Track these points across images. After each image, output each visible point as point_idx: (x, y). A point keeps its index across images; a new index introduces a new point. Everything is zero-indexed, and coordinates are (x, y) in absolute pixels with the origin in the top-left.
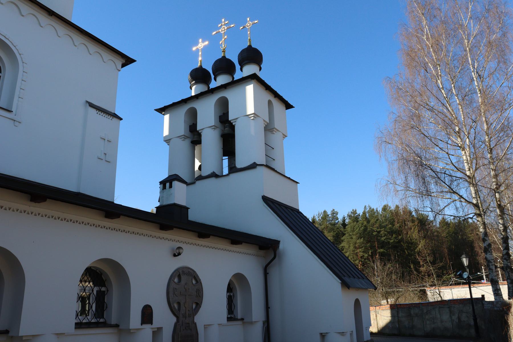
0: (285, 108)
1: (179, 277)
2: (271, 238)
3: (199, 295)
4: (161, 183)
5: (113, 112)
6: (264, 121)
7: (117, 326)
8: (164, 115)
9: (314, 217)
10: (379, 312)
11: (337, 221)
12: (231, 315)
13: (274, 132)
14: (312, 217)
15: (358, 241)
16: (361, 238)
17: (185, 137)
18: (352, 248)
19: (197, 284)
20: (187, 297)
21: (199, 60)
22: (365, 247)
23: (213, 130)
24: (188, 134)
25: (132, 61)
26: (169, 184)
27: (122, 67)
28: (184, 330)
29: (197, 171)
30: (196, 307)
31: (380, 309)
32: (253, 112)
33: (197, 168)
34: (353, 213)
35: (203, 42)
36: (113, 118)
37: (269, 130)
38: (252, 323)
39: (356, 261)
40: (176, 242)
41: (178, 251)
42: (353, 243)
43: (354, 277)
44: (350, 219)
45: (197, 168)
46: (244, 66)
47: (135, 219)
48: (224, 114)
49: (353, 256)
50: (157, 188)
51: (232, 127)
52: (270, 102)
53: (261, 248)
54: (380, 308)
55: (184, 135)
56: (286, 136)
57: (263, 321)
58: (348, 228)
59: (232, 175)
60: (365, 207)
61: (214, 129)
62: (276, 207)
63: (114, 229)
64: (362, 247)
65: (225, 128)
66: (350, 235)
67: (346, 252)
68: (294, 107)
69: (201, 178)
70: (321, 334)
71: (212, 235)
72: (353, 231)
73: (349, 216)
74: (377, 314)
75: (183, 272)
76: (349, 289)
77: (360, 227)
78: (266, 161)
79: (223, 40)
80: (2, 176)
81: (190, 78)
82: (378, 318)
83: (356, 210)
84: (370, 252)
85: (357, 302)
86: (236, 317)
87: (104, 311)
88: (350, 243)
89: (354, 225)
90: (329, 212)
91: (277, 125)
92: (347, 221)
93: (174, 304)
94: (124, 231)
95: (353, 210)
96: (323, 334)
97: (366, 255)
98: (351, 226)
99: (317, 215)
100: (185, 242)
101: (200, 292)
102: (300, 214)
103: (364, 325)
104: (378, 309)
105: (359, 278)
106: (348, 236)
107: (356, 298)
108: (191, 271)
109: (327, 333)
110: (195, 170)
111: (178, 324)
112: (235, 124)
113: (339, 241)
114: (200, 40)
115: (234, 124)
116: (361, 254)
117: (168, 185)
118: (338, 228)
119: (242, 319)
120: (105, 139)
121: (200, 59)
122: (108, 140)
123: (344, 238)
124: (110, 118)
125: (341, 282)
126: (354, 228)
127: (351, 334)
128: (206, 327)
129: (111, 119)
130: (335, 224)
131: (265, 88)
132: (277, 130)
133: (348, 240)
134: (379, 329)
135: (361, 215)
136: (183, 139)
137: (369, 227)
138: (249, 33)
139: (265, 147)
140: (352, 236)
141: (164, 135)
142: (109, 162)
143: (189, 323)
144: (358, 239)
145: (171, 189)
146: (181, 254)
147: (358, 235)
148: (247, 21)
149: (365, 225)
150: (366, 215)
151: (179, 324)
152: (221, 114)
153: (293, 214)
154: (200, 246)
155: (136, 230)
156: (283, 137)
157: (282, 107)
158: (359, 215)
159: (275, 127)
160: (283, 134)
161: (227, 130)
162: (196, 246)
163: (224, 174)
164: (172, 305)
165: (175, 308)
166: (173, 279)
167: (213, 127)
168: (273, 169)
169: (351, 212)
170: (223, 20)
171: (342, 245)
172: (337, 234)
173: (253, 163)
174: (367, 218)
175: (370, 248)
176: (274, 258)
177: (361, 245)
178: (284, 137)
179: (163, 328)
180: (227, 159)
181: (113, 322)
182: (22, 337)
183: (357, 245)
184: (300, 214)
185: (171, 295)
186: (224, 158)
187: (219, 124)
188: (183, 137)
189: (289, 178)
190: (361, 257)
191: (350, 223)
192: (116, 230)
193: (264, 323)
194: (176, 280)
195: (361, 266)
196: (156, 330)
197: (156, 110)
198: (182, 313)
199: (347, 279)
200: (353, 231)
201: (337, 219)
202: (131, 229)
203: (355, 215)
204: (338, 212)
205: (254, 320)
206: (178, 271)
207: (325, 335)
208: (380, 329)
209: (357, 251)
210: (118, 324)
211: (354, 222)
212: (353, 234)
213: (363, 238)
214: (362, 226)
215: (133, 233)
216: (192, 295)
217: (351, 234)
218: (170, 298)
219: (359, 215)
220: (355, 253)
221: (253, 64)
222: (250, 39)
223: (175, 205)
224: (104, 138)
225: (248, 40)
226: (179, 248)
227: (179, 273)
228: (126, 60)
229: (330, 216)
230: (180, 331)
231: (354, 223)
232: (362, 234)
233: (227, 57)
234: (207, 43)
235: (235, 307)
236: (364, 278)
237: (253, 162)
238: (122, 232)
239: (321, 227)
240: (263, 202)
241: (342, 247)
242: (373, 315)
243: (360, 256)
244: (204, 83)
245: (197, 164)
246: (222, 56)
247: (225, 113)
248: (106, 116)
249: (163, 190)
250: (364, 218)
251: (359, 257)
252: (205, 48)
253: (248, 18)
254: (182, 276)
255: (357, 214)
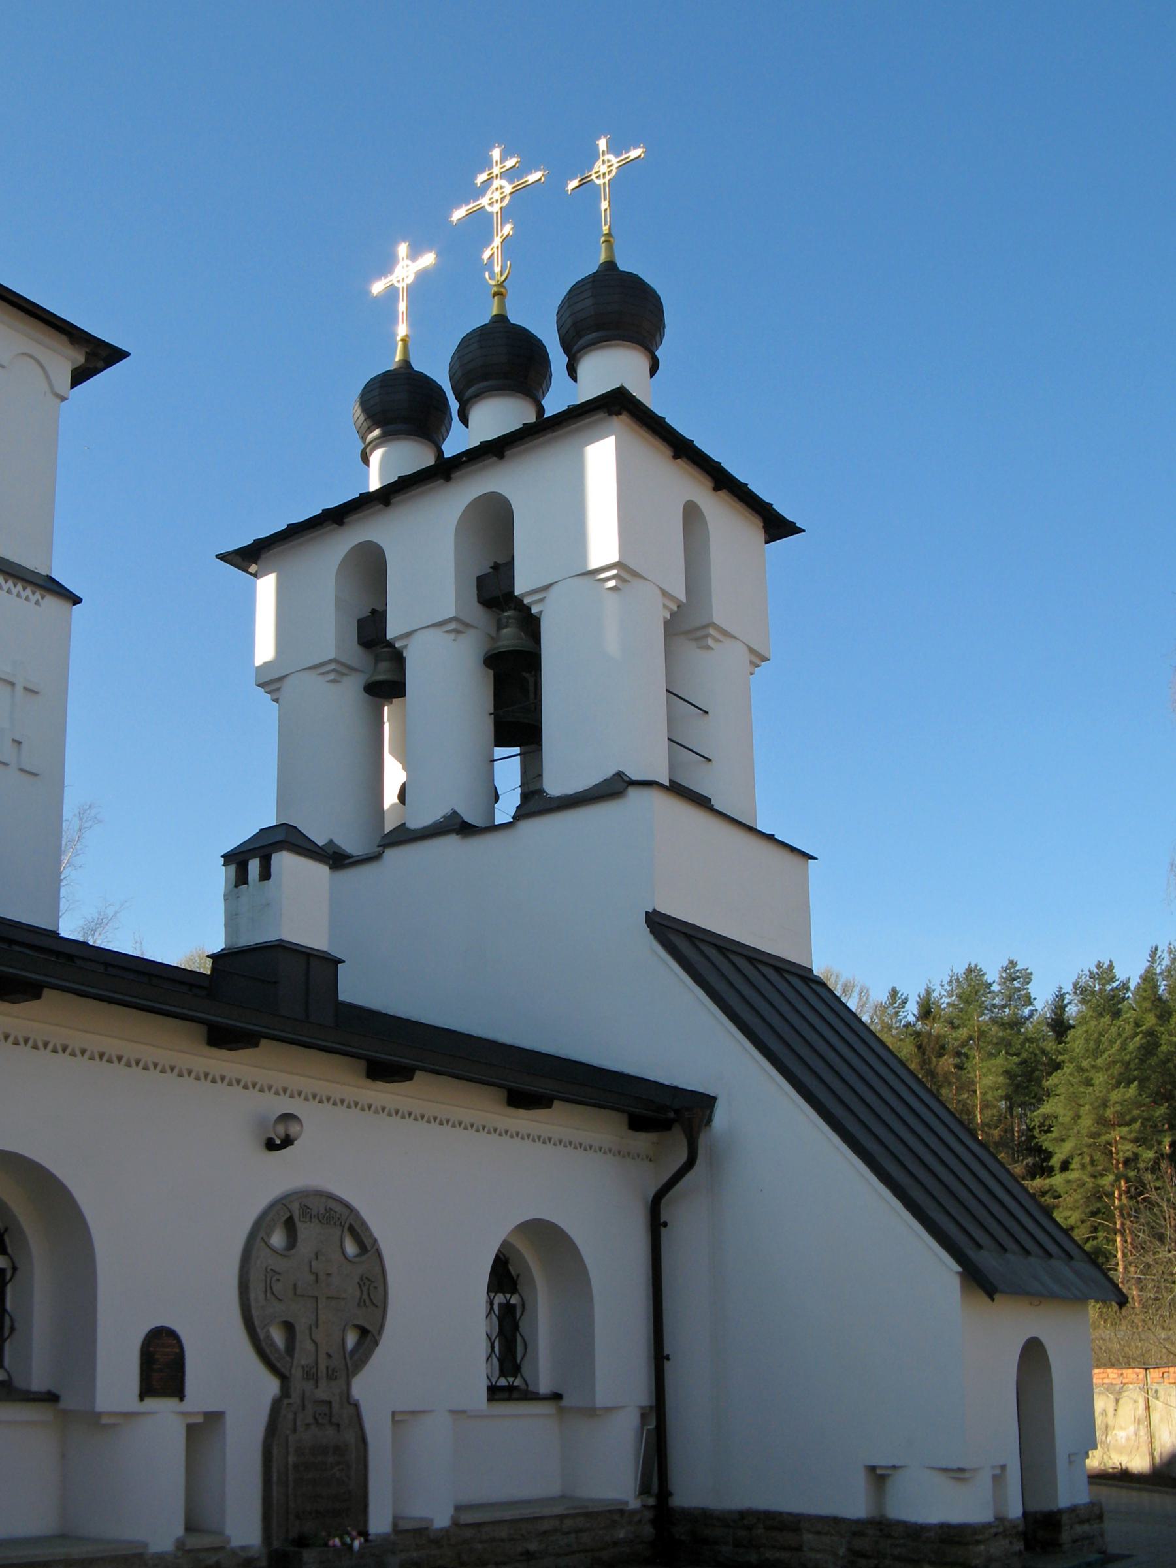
0: (760, 536)
1: (290, 1226)
2: (681, 1086)
3: (371, 1299)
4: (228, 858)
5: (44, 573)
6: (665, 593)
7: (51, 1398)
8: (255, 575)
9: (929, 992)
10: (1161, 1394)
11: (1026, 1011)
12: (511, 1379)
13: (710, 642)
14: (923, 993)
15: (1115, 1096)
16: (1129, 1083)
17: (338, 669)
18: (1087, 1122)
19: (364, 1258)
20: (320, 1306)
21: (399, 338)
22: (1147, 1120)
23: (452, 636)
24: (354, 653)
25: (114, 355)
26: (258, 863)
27: (73, 385)
28: (308, 1425)
29: (393, 806)
30: (359, 1344)
31: (1166, 1381)
32: (615, 558)
33: (390, 797)
34: (1100, 979)
35: (414, 255)
36: (43, 598)
37: (687, 633)
38: (591, 1412)
39: (1102, 1175)
40: (277, 1093)
41: (281, 1130)
42: (1091, 1104)
43: (1000, 1245)
44: (1083, 1001)
45: (390, 797)
46: (581, 357)
47: (105, 1004)
48: (496, 567)
49: (1092, 1157)
50: (219, 876)
51: (531, 624)
52: (691, 514)
53: (637, 1124)
54: (1165, 1375)
55: (334, 661)
56: (765, 659)
57: (642, 1408)
58: (1076, 1041)
59: (529, 827)
60: (1154, 952)
61: (457, 631)
62: (707, 958)
63: (26, 1041)
64: (1134, 1120)
65: (500, 627)
66: (1081, 1069)
67: (1063, 1140)
68: (803, 531)
69: (403, 836)
70: (872, 1469)
71: (420, 1070)
72: (1096, 1052)
73: (1082, 991)
74: (1153, 1401)
75: (306, 1211)
76: (993, 1300)
77: (1127, 1038)
78: (672, 767)
79: (497, 241)
80: (531, 688)
81: (362, 418)
82: (1155, 1416)
83: (1111, 966)
84: (1167, 1141)
85: (1034, 1351)
86: (531, 1388)
87: (4, 1341)
88: (1081, 1102)
89: (1100, 1028)
90: (992, 975)
91: (722, 610)
92: (1072, 1010)
93: (268, 1331)
94: (64, 1050)
95: (1099, 966)
96: (879, 1472)
97: (1150, 1154)
98: (1087, 1032)
99: (943, 986)
100: (314, 1096)
101: (376, 1288)
102: (814, 986)
103: (1063, 1442)
104: (1155, 1380)
105: (1027, 1253)
106: (1071, 1074)
107: (1029, 1336)
108: (338, 1208)
109: (894, 1467)
110: (386, 806)
111: (286, 1401)
112: (541, 612)
113: (1036, 1095)
114: (403, 249)
115: (534, 610)
116: (1126, 1149)
117: (254, 866)
118: (1030, 1040)
119: (557, 1397)
120: (13, 684)
121: (402, 330)
122: (25, 688)
123: (1056, 1081)
124: (34, 598)
125: (960, 1269)
126: (1098, 1042)
127: (999, 1478)
128: (398, 1419)
129: (37, 603)
130: (1016, 1023)
131: (669, 453)
132: (726, 634)
133: (1071, 1090)
134: (1157, 1460)
135: (1132, 987)
136: (332, 676)
137: (1165, 1037)
138: (604, 205)
139: (669, 705)
140: (1092, 1074)
141: (259, 661)
142: (35, 775)
143: (330, 1403)
144: (1118, 1085)
145: (267, 881)
146: (295, 1143)
147: (1116, 1070)
148: (594, 156)
149: (1151, 1028)
150: (1155, 987)
151: (289, 1404)
152: (485, 568)
153: (783, 986)
154: (376, 1112)
155: (113, 1046)
156: (752, 662)
157: (750, 530)
158: (1125, 987)
159: (715, 621)
160: (752, 651)
161: (510, 637)
162: (358, 1110)
163: (498, 821)
164: (259, 1330)
165: (272, 1344)
166: (262, 1234)
167: (452, 626)
168: (702, 802)
169: (1091, 973)
170: (496, 154)
171: (1046, 1108)
172: (1024, 1062)
173: (614, 775)
174: (1160, 999)
175: (1166, 1126)
176: (690, 1163)
177: (1130, 1111)
178: (757, 661)
179: (229, 1420)
180: (519, 757)
181: (38, 1382)
182: (100, 1414)
183: (1109, 1113)
184: (812, 989)
185: (256, 1293)
186: (499, 752)
187: (476, 613)
188: (332, 666)
189: (770, 838)
190: (1127, 1162)
191: (1083, 1020)
192: (30, 1043)
193: (644, 1416)
194: (277, 1239)
195: (1124, 1197)
196: (200, 1419)
197: (223, 557)
198: (303, 1362)
199: (987, 1260)
200: (1096, 1052)
201: (1029, 1001)
202: (96, 1042)
203: (1109, 987)
204: (1031, 974)
205: (601, 1400)
206: (285, 1205)
207: (888, 1475)
208: (1161, 1459)
209: (1107, 1137)
210: (53, 1389)
211: (1101, 1015)
212: (1094, 1067)
213: (1136, 1083)
214: (1136, 1034)
215: (101, 1056)
216: (344, 1299)
217: (1085, 1064)
218: (253, 1303)
219: (1125, 987)
220: (1100, 1145)
221: (623, 346)
222: (609, 235)
223: (282, 947)
224: (12, 680)
225: (603, 239)
226: (287, 1117)
227: (288, 1214)
228: (86, 353)
229: (995, 988)
230: (295, 1430)
231: (1102, 1020)
232: (1132, 1066)
233: (514, 319)
234: (428, 259)
235: (528, 1355)
236: (1070, 1257)
237: (612, 771)
238: (55, 1051)
239: (954, 1035)
240: (652, 937)
241: (1046, 1117)
242: (1135, 1401)
243: (1121, 1155)
244: (417, 436)
245: (394, 775)
246: (494, 313)
247: (500, 561)
248: (15, 591)
249: (236, 886)
250: (1145, 999)
251: (1118, 1162)
252: (422, 284)
253: (599, 138)
254: (299, 1225)
255: (1117, 983)
